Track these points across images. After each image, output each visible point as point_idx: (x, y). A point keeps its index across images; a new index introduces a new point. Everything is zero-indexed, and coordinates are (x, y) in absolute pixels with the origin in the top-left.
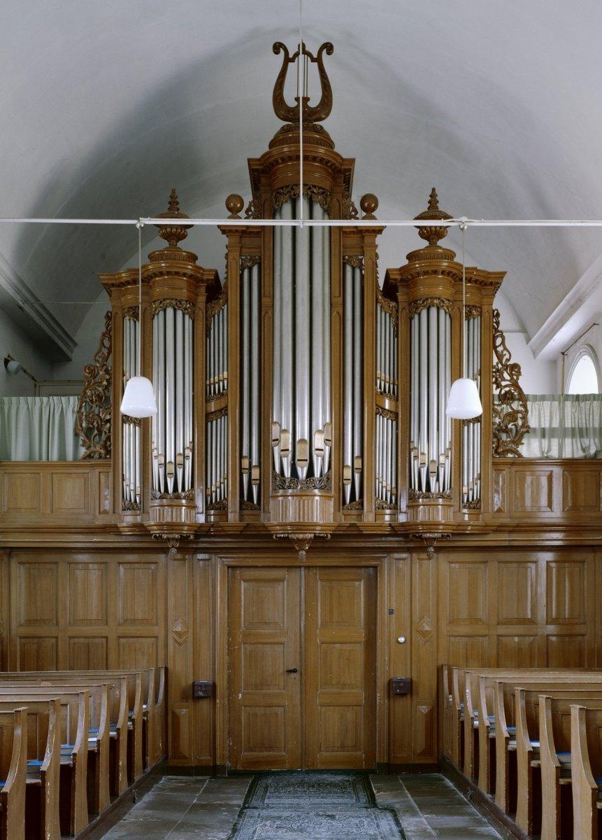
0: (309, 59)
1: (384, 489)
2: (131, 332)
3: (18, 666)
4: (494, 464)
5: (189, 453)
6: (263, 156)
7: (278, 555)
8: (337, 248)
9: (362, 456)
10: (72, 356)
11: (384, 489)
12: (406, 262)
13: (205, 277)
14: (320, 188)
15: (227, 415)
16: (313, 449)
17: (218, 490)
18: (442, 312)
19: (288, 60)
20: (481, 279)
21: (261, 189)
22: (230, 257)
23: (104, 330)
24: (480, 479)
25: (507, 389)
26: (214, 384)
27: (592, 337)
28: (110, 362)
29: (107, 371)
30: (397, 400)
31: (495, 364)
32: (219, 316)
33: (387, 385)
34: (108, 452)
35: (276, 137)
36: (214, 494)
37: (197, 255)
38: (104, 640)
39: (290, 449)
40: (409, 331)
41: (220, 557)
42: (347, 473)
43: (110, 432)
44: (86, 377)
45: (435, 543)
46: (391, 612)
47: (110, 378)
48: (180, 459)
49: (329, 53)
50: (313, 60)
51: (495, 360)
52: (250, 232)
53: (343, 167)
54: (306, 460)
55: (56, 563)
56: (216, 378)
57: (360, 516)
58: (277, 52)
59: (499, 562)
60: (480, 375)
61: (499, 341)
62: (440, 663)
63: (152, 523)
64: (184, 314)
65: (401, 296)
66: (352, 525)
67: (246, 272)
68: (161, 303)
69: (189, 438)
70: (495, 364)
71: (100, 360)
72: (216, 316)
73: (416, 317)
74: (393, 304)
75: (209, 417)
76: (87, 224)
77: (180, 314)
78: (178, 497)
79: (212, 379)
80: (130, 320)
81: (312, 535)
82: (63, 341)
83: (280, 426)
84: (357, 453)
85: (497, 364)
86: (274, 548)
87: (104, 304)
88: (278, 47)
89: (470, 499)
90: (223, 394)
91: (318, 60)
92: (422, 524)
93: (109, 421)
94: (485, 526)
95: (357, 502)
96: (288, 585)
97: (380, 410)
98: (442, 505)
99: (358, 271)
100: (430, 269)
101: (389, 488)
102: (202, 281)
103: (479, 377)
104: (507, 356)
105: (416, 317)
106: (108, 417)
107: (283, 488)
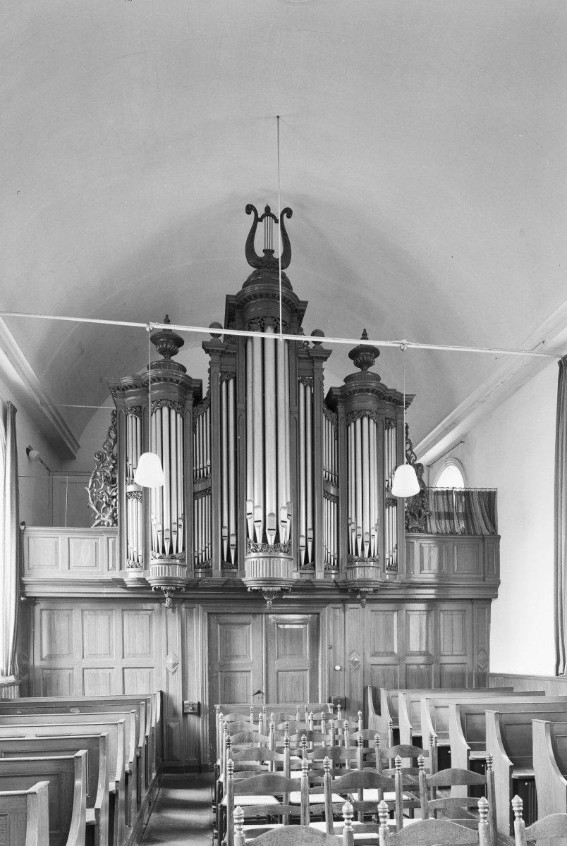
2: (132, 424)
3: (42, 692)
5: (181, 522)
6: (238, 294)
7: (239, 604)
8: (294, 369)
10: (77, 455)
11: (332, 558)
12: (344, 384)
13: (193, 386)
15: (211, 494)
16: (280, 521)
17: (204, 553)
18: (372, 421)
19: (257, 220)
21: (236, 320)
22: (212, 372)
23: (111, 424)
26: (200, 469)
27: (458, 452)
28: (115, 450)
29: (113, 457)
30: (338, 487)
32: (203, 417)
34: (115, 522)
35: (249, 279)
36: (200, 556)
37: (186, 367)
40: (346, 439)
41: (333, 608)
42: (302, 541)
43: (116, 506)
44: (97, 462)
45: (368, 597)
47: (116, 463)
48: (174, 527)
49: (289, 217)
52: (228, 353)
53: (299, 308)
56: (201, 465)
57: (313, 574)
58: (249, 213)
62: (366, 685)
64: (176, 413)
65: (340, 409)
66: (307, 581)
67: (224, 384)
68: (158, 403)
69: (181, 512)
71: (107, 448)
73: (353, 424)
74: (334, 414)
75: (196, 495)
76: (105, 324)
77: (173, 412)
79: (198, 466)
80: (132, 416)
81: (279, 588)
82: (70, 442)
83: (254, 503)
84: (310, 526)
86: (244, 599)
87: (109, 407)
88: (250, 209)
90: (207, 478)
92: (358, 581)
93: (115, 497)
95: (309, 563)
96: (253, 628)
99: (308, 388)
100: (364, 388)
101: (332, 554)
102: (190, 388)
104: (414, 458)
105: (353, 424)
106: (114, 494)
107: (256, 551)
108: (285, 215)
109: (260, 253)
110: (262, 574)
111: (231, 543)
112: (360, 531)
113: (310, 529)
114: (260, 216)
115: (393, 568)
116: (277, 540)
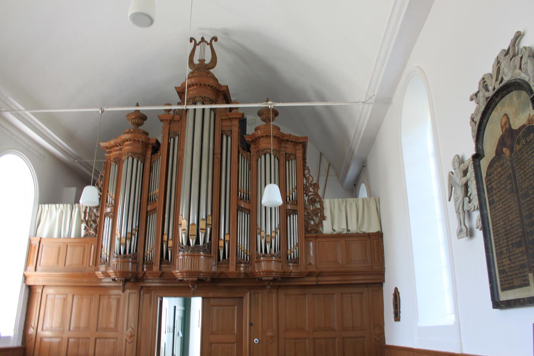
0: (206, 44)
1: (243, 253)
4: (306, 237)
9: (229, 234)
11: (243, 253)
14: (208, 98)
16: (200, 229)
19: (196, 45)
20: (294, 140)
24: (298, 246)
25: (312, 196)
31: (305, 183)
33: (245, 195)
38: (98, 340)
39: (187, 229)
42: (221, 243)
46: (251, 325)
48: (273, 234)
50: (208, 44)
51: (305, 181)
54: (195, 235)
55: (47, 296)
59: (313, 294)
60: (297, 189)
61: (306, 172)
63: (178, 271)
70: (305, 183)
72: (156, 161)
74: (249, 153)
78: (273, 256)
79: (152, 193)
84: (227, 232)
85: (306, 183)
88: (192, 39)
89: (292, 257)
91: (211, 44)
94: (301, 273)
97: (239, 209)
98: (274, 261)
101: (245, 252)
103: (296, 190)
104: (311, 179)
108: (213, 41)
109: (196, 61)
110: (187, 268)
111: (169, 246)
112: (263, 234)
113: (227, 234)
114: (197, 43)
115: (296, 261)
116: (197, 242)
